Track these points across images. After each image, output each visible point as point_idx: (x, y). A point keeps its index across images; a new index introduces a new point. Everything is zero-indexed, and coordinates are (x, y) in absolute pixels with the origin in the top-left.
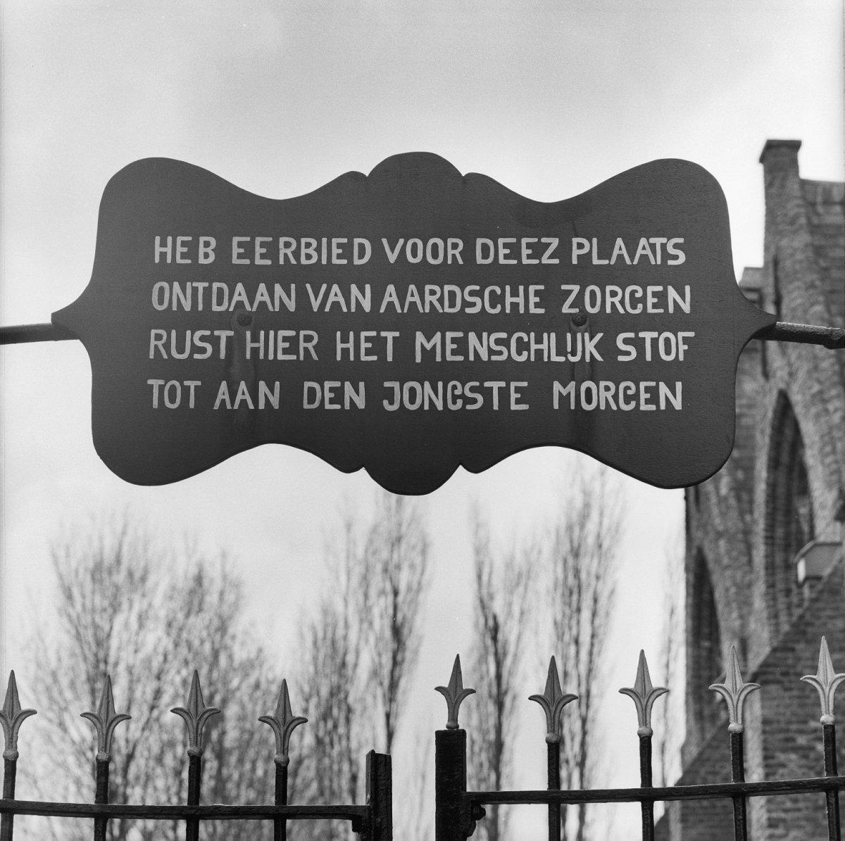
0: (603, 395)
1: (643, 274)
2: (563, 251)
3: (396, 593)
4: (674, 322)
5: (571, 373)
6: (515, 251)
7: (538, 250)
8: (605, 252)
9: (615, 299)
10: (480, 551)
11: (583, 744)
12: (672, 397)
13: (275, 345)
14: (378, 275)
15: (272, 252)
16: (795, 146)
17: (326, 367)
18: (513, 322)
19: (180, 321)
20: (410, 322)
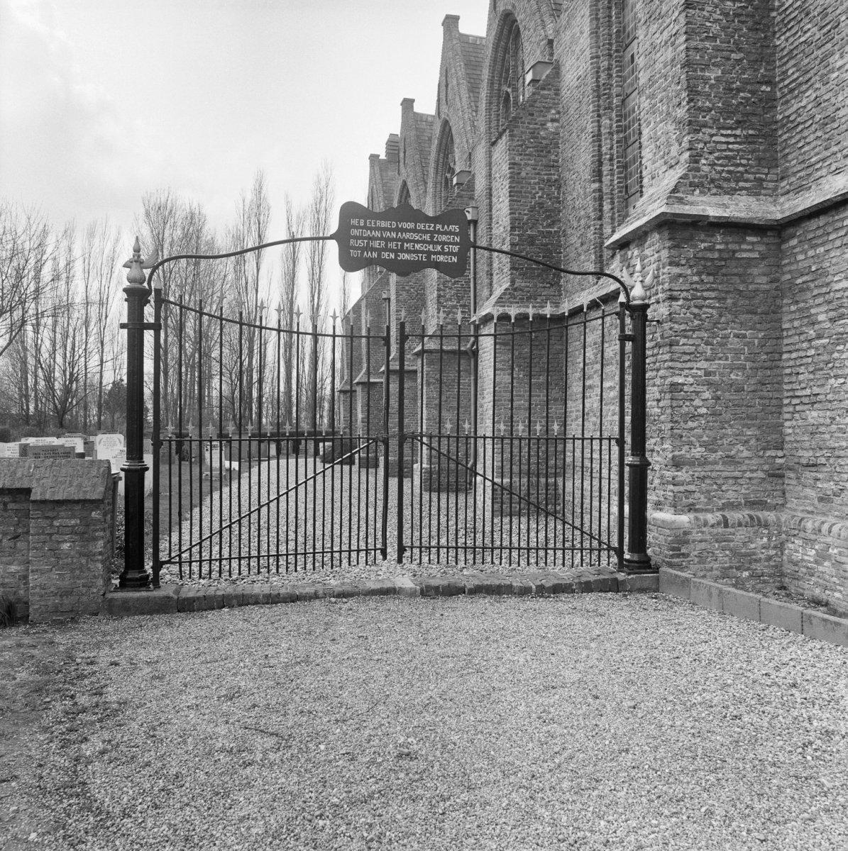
0: (441, 258)
1: (450, 233)
2: (435, 227)
3: (259, 224)
4: (456, 244)
5: (435, 253)
6: (425, 227)
7: (429, 227)
8: (443, 228)
9: (444, 238)
10: (288, 211)
11: (320, 276)
12: (455, 259)
13: (376, 244)
14: (397, 230)
15: (375, 224)
16: (413, 101)
17: (386, 249)
18: (424, 242)
19: (357, 238)
20: (404, 241)
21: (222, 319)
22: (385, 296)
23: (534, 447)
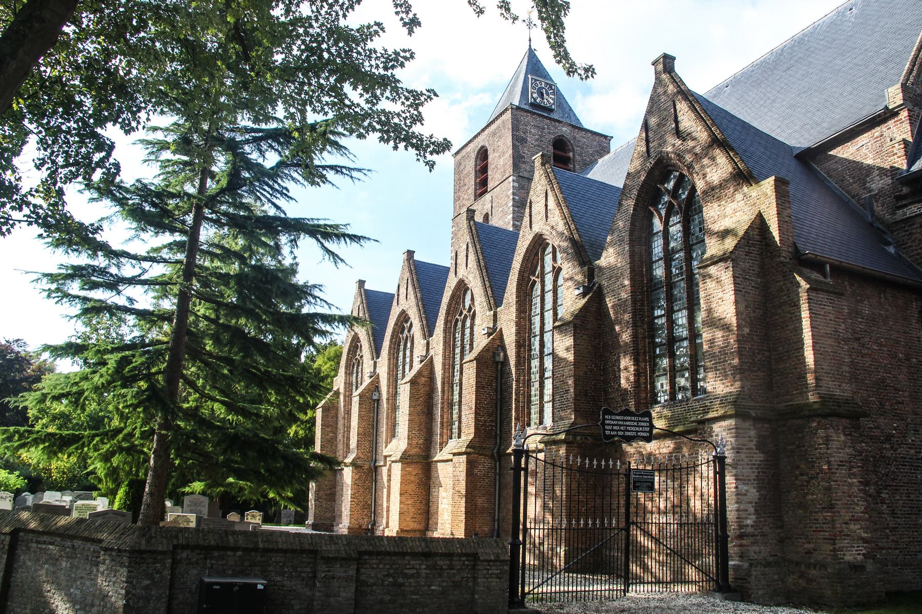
1: (645, 421)
9: (642, 424)
14: (624, 420)
18: (635, 426)
21: (554, 465)
22: (375, 397)
23: (572, 533)
